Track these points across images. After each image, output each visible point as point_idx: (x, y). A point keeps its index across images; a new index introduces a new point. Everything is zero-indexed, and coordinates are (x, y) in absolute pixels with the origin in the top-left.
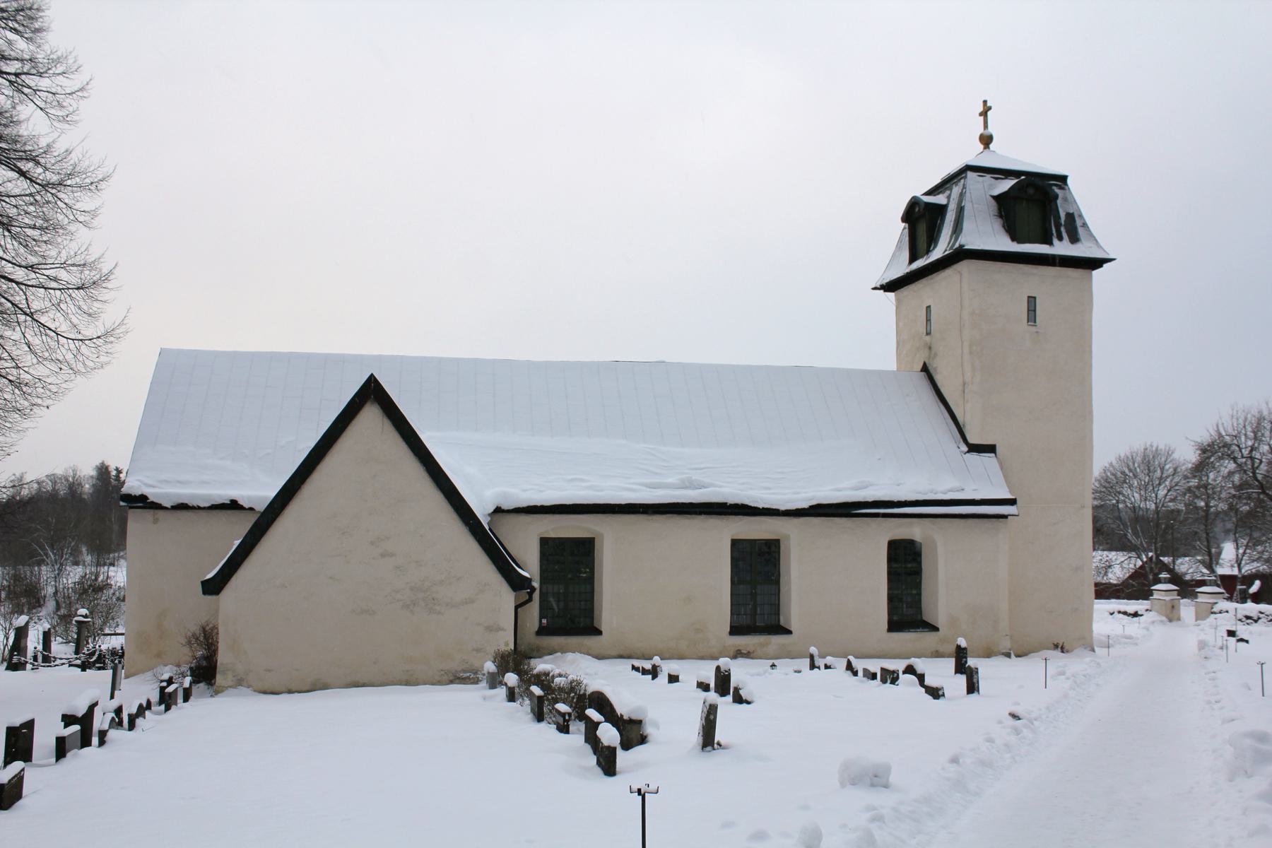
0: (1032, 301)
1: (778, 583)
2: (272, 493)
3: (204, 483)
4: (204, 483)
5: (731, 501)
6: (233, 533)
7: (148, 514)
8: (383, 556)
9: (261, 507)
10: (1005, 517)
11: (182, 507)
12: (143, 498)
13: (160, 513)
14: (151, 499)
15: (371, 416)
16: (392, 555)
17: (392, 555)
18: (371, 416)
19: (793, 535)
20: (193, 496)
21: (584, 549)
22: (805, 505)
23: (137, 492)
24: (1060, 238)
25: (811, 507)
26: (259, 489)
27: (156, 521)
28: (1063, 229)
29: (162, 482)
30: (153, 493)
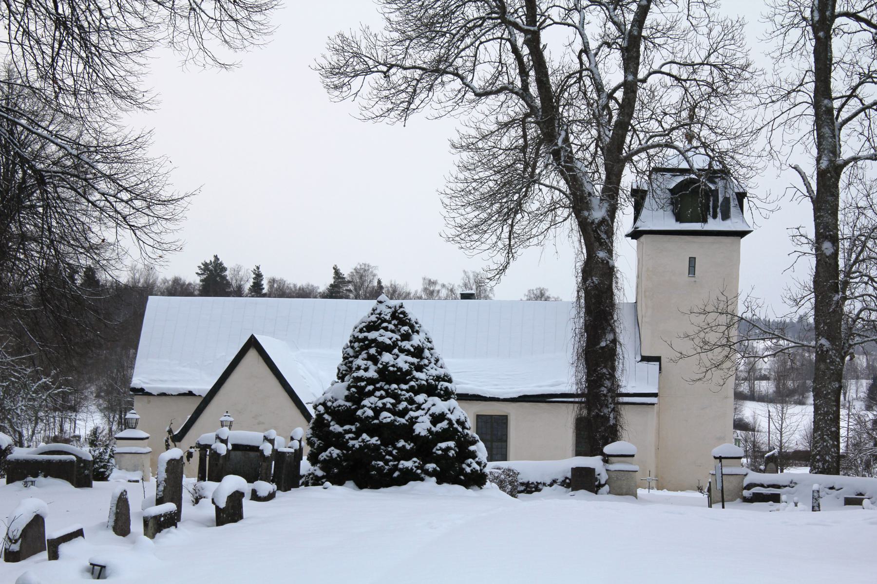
0: (692, 261)
1: (506, 441)
2: (209, 387)
3: (175, 381)
4: (175, 381)
5: (471, 392)
6: (192, 406)
7: (145, 398)
8: (259, 424)
9: (204, 395)
10: (653, 404)
11: (163, 394)
12: (142, 390)
13: (151, 398)
14: (146, 390)
15: (252, 354)
16: (263, 423)
17: (263, 423)
18: (252, 354)
19: (516, 415)
20: (169, 389)
21: (503, 421)
22: (516, 396)
23: (139, 387)
24: (715, 217)
25: (520, 397)
26: (203, 386)
27: (149, 402)
28: (718, 210)
29: (151, 380)
30: (147, 387)
